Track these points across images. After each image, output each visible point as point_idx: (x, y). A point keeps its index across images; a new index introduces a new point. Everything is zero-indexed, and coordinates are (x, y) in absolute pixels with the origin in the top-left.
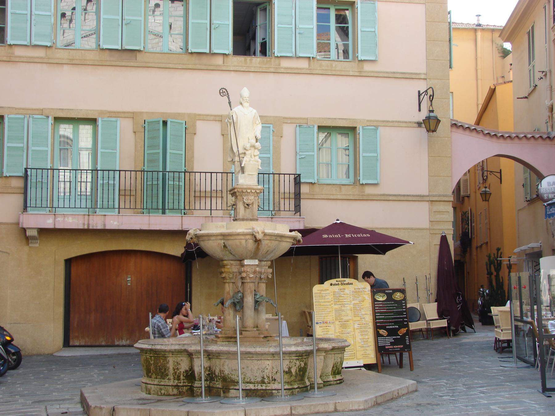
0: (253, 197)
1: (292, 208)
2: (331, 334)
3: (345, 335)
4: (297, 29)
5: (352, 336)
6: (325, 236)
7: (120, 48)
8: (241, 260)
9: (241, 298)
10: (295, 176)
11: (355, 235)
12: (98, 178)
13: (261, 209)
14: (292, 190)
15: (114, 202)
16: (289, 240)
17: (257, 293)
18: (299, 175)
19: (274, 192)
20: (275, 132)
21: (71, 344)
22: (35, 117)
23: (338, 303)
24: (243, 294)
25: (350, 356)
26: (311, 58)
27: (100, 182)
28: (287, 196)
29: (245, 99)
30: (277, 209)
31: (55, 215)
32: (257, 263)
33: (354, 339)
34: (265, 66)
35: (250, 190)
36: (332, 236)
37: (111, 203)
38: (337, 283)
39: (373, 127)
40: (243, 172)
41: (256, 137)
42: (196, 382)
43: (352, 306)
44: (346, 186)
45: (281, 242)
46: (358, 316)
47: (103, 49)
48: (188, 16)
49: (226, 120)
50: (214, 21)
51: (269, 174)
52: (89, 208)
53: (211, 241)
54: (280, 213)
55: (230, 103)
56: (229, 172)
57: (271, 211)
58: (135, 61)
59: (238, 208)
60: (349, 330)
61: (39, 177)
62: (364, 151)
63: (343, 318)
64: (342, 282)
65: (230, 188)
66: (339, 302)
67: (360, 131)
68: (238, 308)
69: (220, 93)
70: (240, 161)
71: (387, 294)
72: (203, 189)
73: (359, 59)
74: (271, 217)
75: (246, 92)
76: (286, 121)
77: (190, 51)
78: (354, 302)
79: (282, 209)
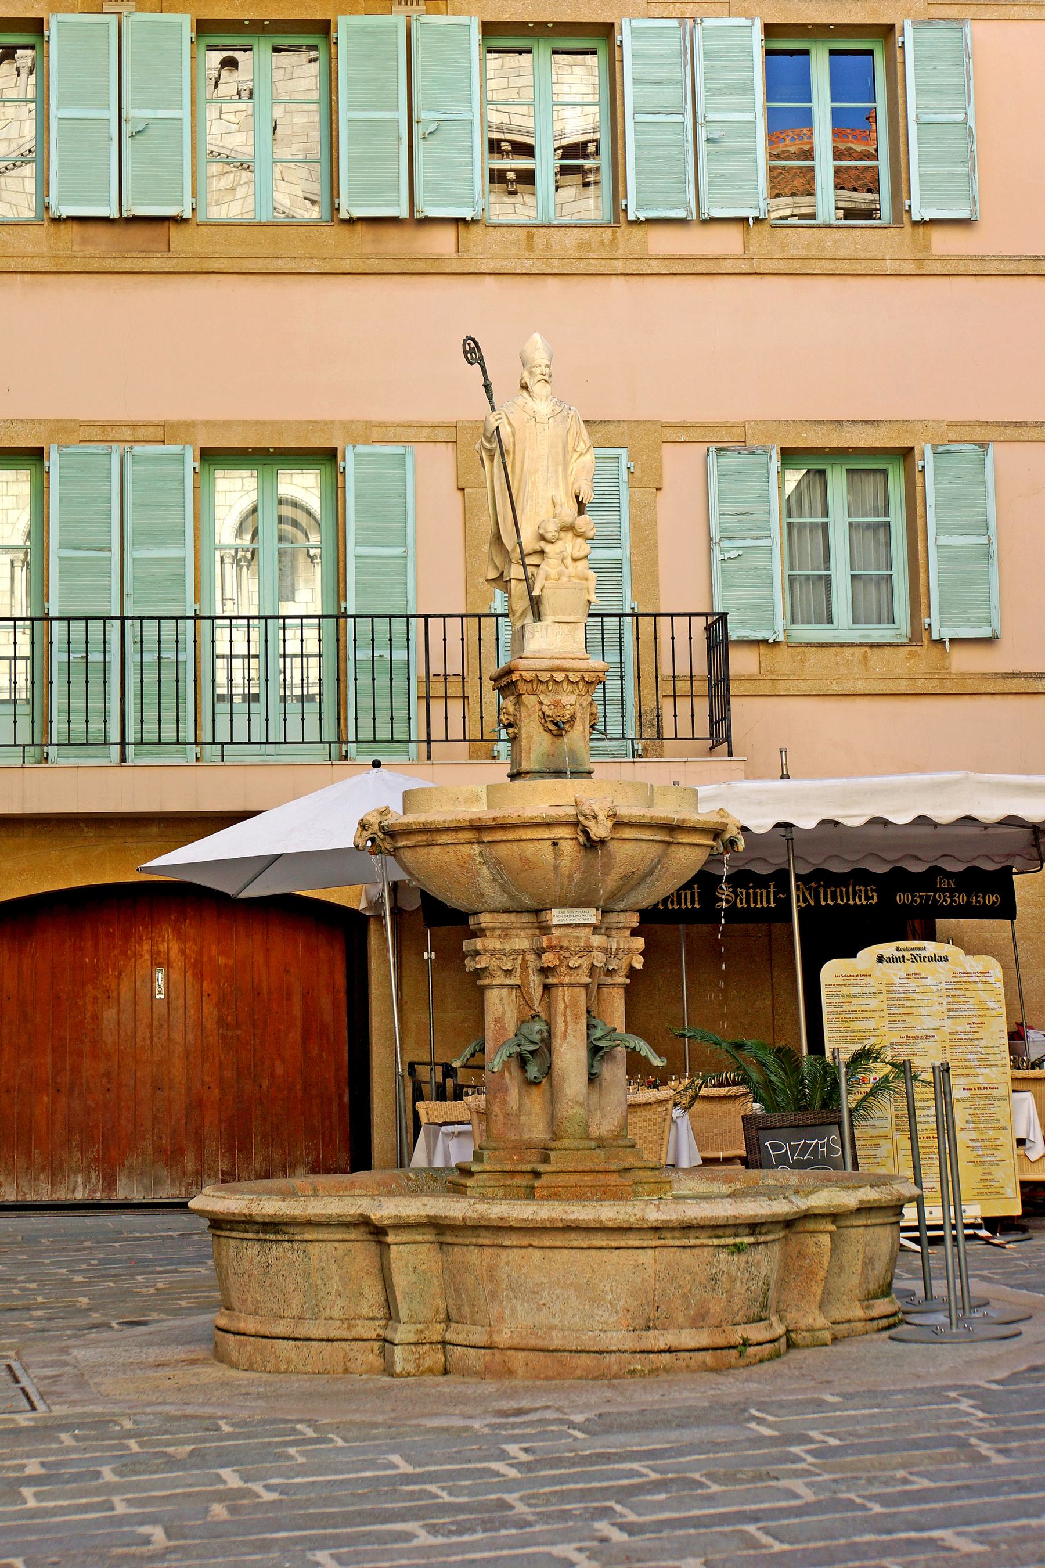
0: (572, 699)
1: (703, 727)
2: (881, 1118)
4: (699, 128)
7: (115, 215)
8: (537, 912)
9: (543, 1040)
10: (710, 620)
12: (51, 643)
13: (597, 733)
14: (701, 668)
15: (105, 721)
16: (697, 839)
17: (594, 1022)
18: (723, 617)
19: (639, 677)
20: (638, 474)
24: (548, 1024)
26: (751, 220)
27: (59, 657)
28: (683, 686)
29: (538, 370)
30: (650, 732)
32: (594, 920)
35: (563, 675)
37: (96, 726)
38: (899, 954)
39: (971, 447)
40: (538, 617)
41: (577, 497)
42: (401, 1327)
44: (887, 650)
45: (673, 848)
47: (57, 220)
48: (334, 98)
49: (477, 446)
51: (620, 616)
52: (24, 746)
53: (436, 850)
54: (662, 746)
55: (487, 387)
56: (487, 612)
57: (632, 740)
59: (524, 736)
62: (943, 529)
64: (914, 953)
65: (491, 669)
67: (927, 460)
68: (533, 1071)
69: (465, 353)
70: (527, 580)
72: (682, 669)
73: (916, 217)
74: (631, 760)
75: (538, 348)
77: (343, 215)
79: (668, 731)
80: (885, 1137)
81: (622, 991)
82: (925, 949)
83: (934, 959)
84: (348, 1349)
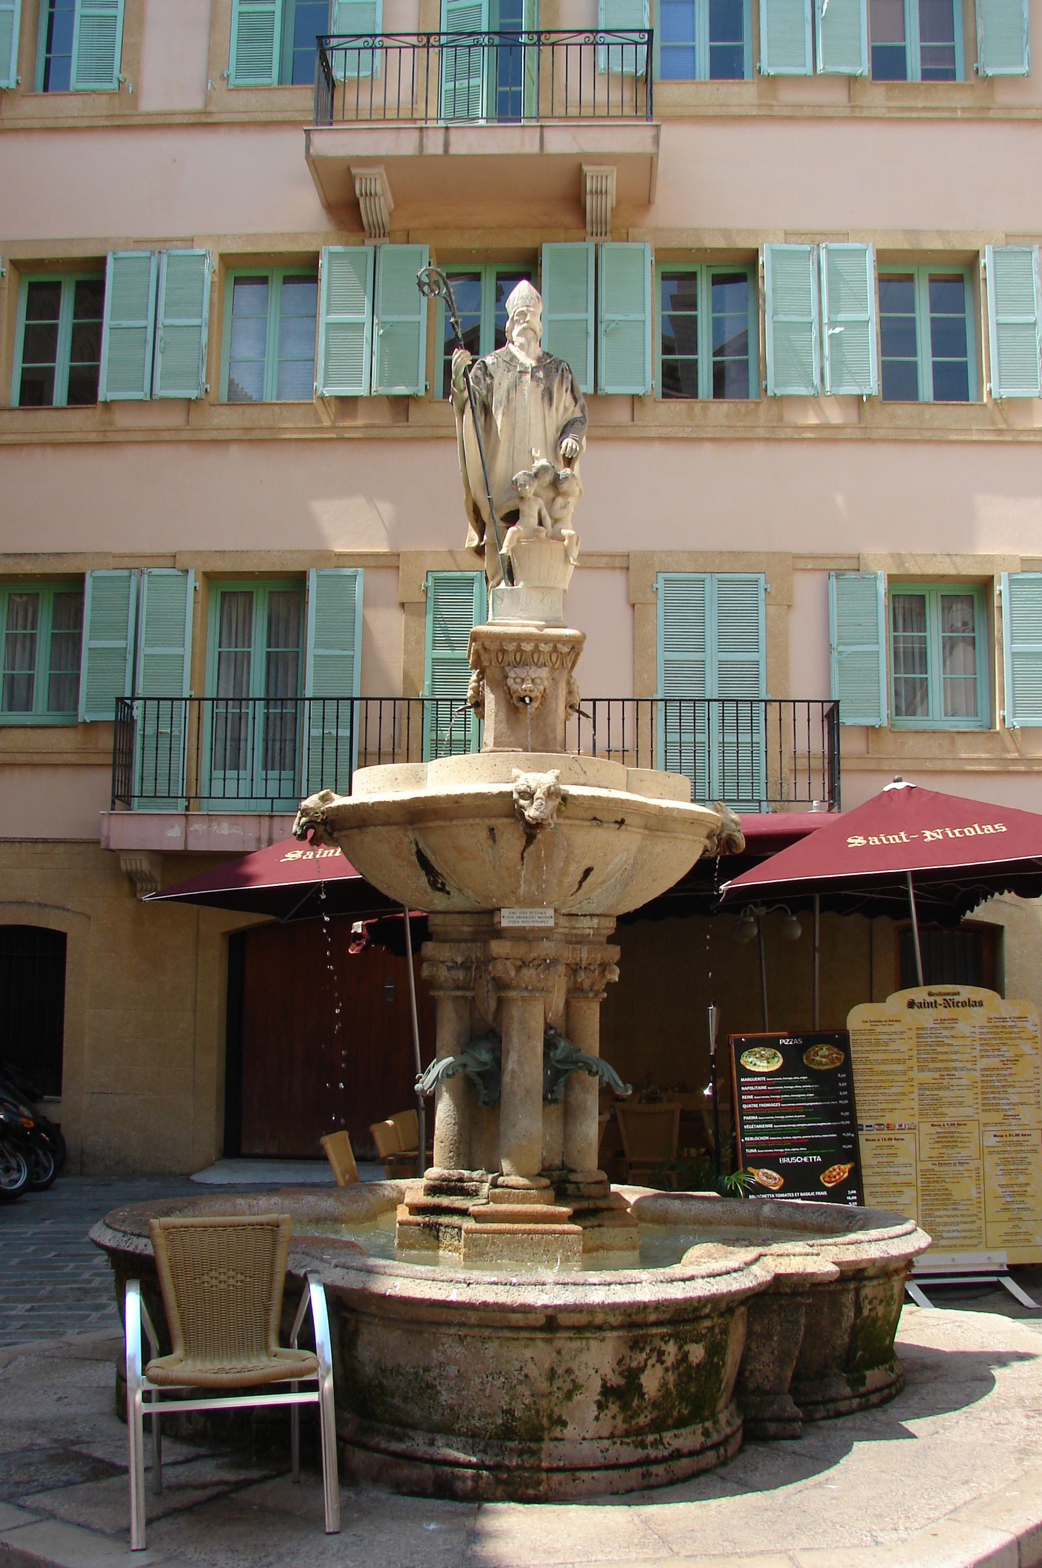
0: (544, 673)
2: (905, 1165)
3: (953, 1168)
5: (973, 1174)
6: (857, 841)
11: (956, 831)
18: (837, 702)
21: (244, 1149)
22: (152, 574)
23: (932, 1065)
25: (965, 1237)
28: (802, 763)
31: (186, 816)
33: (981, 1182)
34: (741, 424)
35: (515, 644)
36: (880, 840)
38: (931, 999)
43: (977, 1075)
46: (998, 1110)
50: (605, 316)
52: (273, 799)
58: (405, 424)
60: (965, 1153)
61: (165, 720)
63: (944, 1110)
64: (947, 998)
66: (934, 1060)
71: (783, 1049)
72: (802, 746)
76: (801, 564)
78: (983, 1063)
80: (908, 1184)
82: (958, 994)
83: (968, 1004)
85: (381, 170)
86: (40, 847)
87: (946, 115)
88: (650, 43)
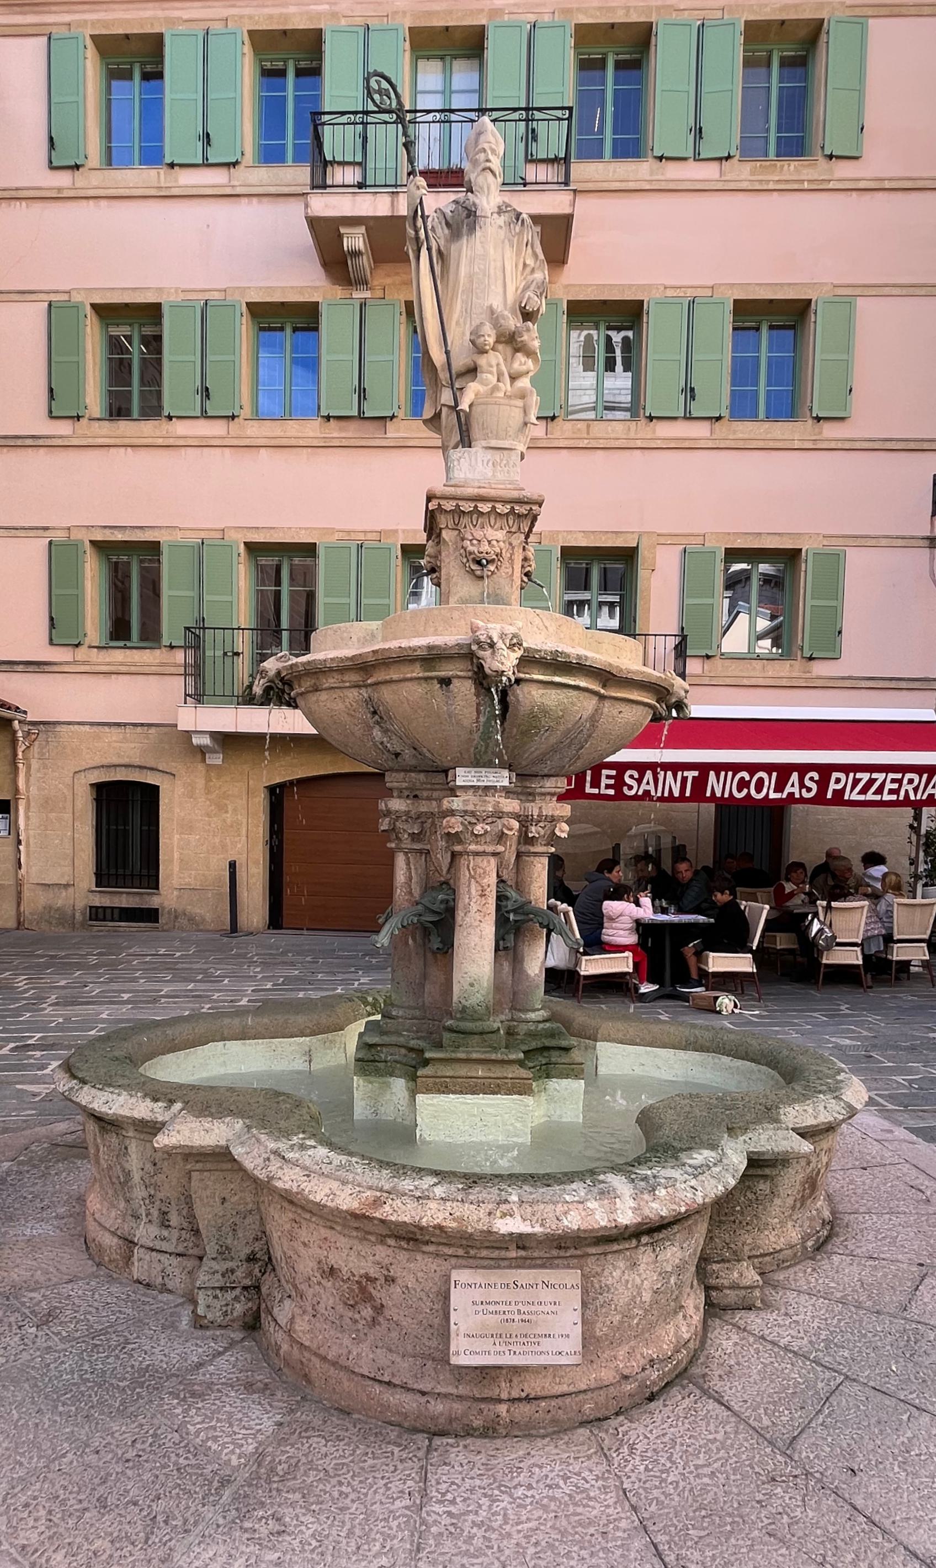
32: (506, 783)
53: (323, 696)
76: (662, 540)
81: (545, 861)
84: (167, 1263)
85: (362, 229)
86: (139, 729)
87: (796, 186)
88: (569, 119)
